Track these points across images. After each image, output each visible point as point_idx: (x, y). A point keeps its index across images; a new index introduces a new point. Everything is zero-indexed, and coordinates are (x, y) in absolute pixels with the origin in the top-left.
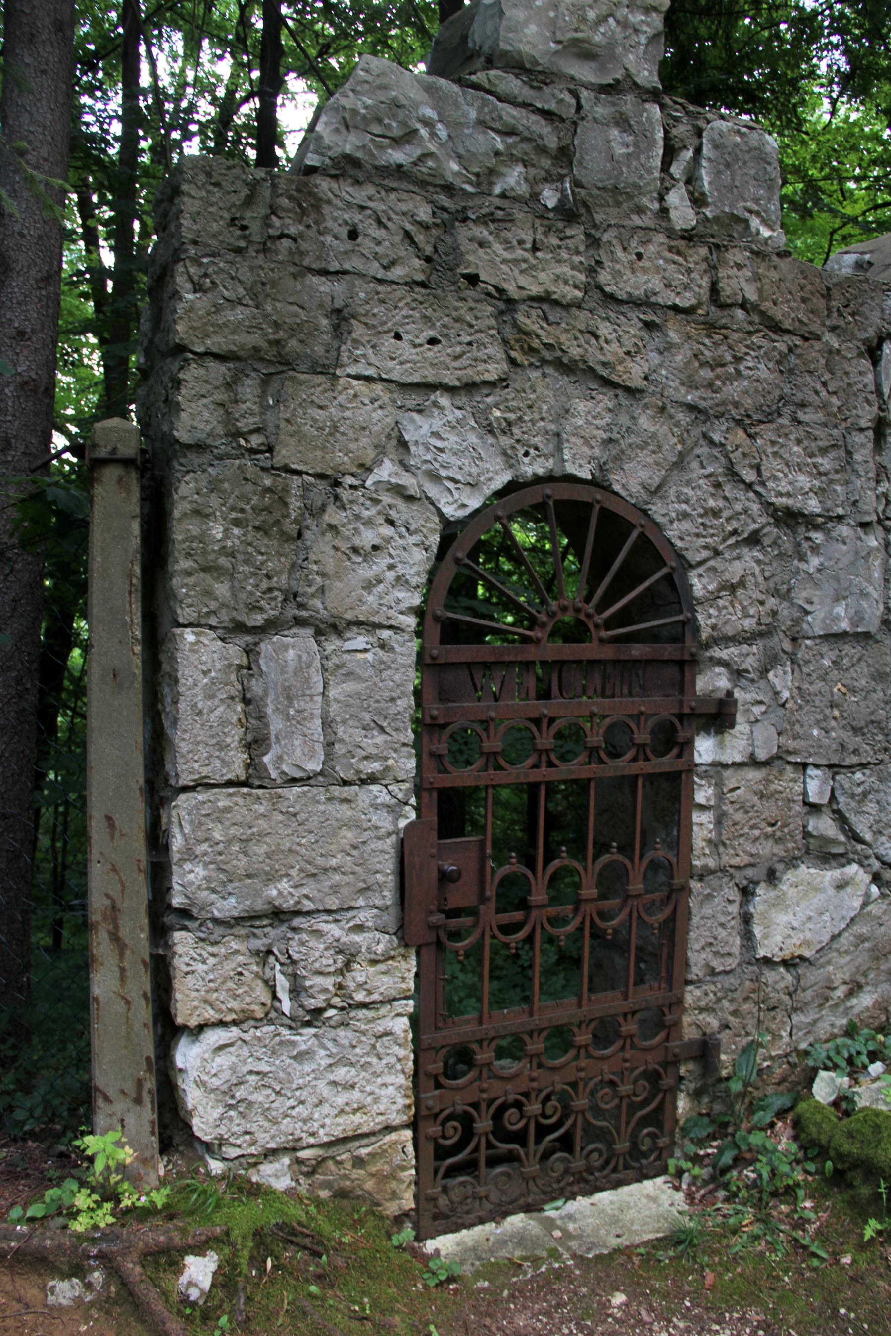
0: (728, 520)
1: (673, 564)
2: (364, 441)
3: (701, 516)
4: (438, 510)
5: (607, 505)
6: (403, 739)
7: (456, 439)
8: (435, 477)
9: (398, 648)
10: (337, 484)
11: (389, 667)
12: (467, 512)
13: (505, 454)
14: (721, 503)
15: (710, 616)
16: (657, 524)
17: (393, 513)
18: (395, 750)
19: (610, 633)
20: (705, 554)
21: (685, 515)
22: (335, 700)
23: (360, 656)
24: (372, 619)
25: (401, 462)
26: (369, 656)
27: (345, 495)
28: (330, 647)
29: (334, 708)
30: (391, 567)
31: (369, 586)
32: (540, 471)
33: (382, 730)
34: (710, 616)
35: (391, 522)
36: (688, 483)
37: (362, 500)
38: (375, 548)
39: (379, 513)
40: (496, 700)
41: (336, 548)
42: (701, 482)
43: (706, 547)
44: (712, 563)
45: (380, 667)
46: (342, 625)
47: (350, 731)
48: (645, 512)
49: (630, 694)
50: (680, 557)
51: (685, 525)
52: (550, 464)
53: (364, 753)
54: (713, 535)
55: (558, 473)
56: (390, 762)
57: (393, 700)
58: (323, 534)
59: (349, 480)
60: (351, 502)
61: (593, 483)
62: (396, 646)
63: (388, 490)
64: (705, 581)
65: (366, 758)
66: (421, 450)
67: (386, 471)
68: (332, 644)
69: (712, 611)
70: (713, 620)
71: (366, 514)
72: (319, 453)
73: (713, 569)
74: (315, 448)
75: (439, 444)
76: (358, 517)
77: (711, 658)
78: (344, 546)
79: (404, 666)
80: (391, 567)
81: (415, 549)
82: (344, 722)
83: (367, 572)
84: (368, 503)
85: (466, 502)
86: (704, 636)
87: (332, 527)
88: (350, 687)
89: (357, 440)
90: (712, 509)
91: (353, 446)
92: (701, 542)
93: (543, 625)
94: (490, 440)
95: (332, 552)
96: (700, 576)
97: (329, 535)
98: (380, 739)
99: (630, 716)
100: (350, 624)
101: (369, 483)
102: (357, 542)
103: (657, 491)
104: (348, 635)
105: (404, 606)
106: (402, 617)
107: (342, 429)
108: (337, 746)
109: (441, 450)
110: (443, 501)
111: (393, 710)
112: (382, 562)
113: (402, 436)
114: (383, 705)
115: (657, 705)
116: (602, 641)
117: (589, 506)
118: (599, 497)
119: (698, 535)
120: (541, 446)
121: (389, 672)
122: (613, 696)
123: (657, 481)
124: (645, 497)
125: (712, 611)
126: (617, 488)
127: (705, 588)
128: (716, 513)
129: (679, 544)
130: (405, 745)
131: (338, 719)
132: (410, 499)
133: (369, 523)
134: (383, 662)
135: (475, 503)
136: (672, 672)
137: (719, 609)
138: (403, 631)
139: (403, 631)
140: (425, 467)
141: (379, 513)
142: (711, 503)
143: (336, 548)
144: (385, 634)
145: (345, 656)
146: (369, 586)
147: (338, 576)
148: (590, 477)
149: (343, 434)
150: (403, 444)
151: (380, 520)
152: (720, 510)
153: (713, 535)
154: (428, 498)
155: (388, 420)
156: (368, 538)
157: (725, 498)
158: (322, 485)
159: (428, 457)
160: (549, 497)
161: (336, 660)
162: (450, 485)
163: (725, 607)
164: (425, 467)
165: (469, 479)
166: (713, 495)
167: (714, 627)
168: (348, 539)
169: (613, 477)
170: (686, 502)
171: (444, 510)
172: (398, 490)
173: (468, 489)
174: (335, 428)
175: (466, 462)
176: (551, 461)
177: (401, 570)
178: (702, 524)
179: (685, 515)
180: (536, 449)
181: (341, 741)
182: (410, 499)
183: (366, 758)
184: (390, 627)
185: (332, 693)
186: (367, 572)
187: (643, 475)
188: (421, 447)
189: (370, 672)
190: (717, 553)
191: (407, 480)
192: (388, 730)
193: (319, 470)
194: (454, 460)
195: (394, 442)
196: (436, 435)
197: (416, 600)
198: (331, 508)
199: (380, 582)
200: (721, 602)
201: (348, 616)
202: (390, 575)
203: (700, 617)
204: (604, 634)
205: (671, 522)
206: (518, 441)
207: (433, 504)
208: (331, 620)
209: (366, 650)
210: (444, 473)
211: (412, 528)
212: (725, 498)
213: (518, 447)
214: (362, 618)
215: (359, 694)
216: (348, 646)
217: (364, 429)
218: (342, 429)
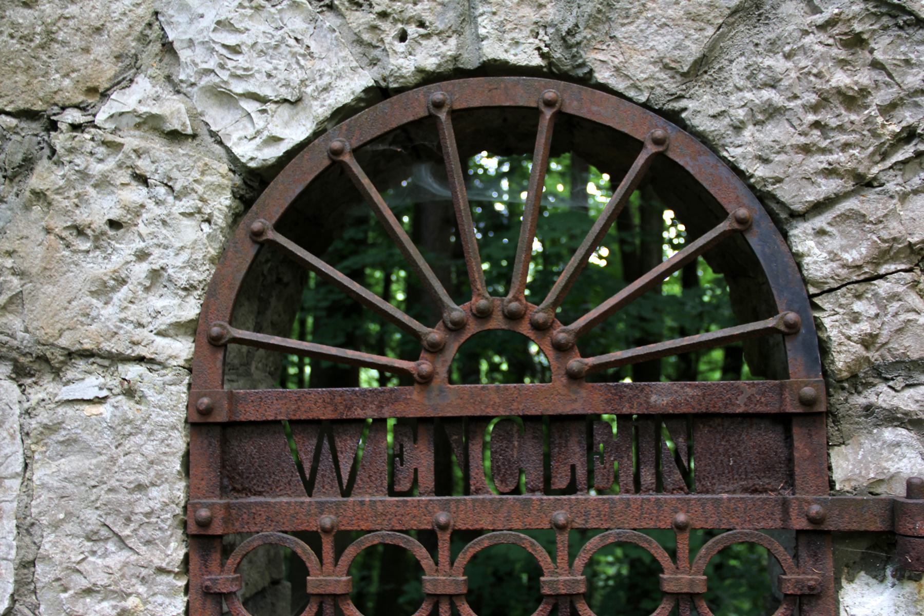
0: (889, 109)
1: (742, 212)
2: (99, 50)
3: (815, 108)
4: (228, 151)
5: (572, 108)
6: (158, 561)
7: (264, 27)
8: (224, 97)
9: (152, 396)
10: (53, 126)
11: (139, 430)
12: (278, 151)
13: (360, 42)
14: (865, 77)
15: (856, 318)
16: (702, 137)
17: (144, 165)
18: (143, 580)
19: (592, 361)
20: (828, 187)
21: (772, 112)
22: (43, 485)
23: (89, 410)
24: (106, 346)
25: (168, 78)
26: (105, 410)
27: (60, 140)
28: (36, 395)
29: (41, 500)
30: (142, 256)
31: (103, 290)
32: (430, 63)
33: (122, 541)
34: (856, 318)
35: (142, 180)
36: (773, 47)
37: (90, 146)
38: (114, 224)
39: (120, 166)
40: (346, 493)
41: (48, 231)
42: (807, 40)
43: (830, 172)
44: (851, 204)
45: (125, 430)
46: (58, 357)
47: (67, 541)
48: (674, 117)
49: (660, 487)
50: (764, 198)
51: (777, 131)
52: (450, 47)
53: (85, 583)
54: (846, 146)
55: (470, 61)
56: (131, 602)
57: (140, 487)
58: (27, 208)
59: (74, 116)
60: (71, 151)
61: (550, 71)
62: (149, 393)
63: (138, 126)
64: (834, 243)
65: (88, 591)
66: (199, 54)
67: (138, 96)
68: (46, 389)
69: (858, 306)
70: (865, 327)
71: (97, 169)
72: (21, 78)
73: (859, 217)
74: (15, 70)
75: (232, 39)
76: (84, 175)
77: (869, 409)
78: (59, 224)
79: (161, 427)
80: (142, 256)
81: (186, 222)
82: (56, 526)
83: (98, 267)
84: (101, 151)
85: (278, 132)
86: (841, 361)
87: (39, 195)
88: (72, 463)
89: (86, 50)
90: (839, 92)
91: (79, 61)
92: (818, 162)
93: (436, 349)
94: (330, 20)
95: (41, 236)
96: (821, 233)
97: (37, 209)
98: (117, 558)
99: (657, 533)
100: (70, 355)
101: (100, 118)
102: (82, 217)
103: (700, 69)
104: (70, 375)
105: (162, 322)
106: (160, 340)
107: (61, 36)
108: (39, 568)
109: (235, 50)
110: (235, 137)
111: (143, 507)
112: (124, 248)
113: (165, 36)
114: (123, 496)
115: (728, 507)
116: (574, 377)
117: (534, 113)
118: (550, 95)
119: (806, 149)
120: (428, 18)
121: (138, 439)
122: (572, 489)
123: (694, 50)
124: (672, 87)
125: (858, 306)
126: (603, 76)
127: (834, 257)
128: (852, 99)
129: (760, 171)
130: (161, 570)
131: (45, 520)
132: (175, 136)
133: (103, 183)
134: (127, 421)
135: (296, 131)
136: (768, 439)
137: (882, 303)
138: (163, 365)
139: (163, 365)
140: (205, 81)
141: (120, 166)
142: (840, 79)
143: (48, 231)
144: (133, 371)
145: (61, 410)
146: (103, 290)
147: (47, 273)
148: (537, 61)
149: (64, 43)
150: (168, 48)
151: (124, 177)
152: (864, 92)
153: (846, 146)
154: (213, 134)
155: (140, 11)
156: (101, 208)
157: (876, 65)
158: (30, 128)
159: (212, 64)
160: (438, 105)
161: (43, 417)
162: (251, 106)
163: (895, 297)
164: (205, 81)
165: (285, 93)
166: (842, 63)
167: (868, 341)
168: (66, 212)
169: (591, 57)
170: (773, 84)
171: (237, 151)
172: (151, 123)
173: (285, 110)
174: (50, 37)
175: (282, 65)
176: (453, 42)
177: (157, 260)
178: (816, 125)
179: (772, 112)
180: (422, 24)
181: (47, 559)
182: (175, 136)
183: (88, 591)
184: (141, 359)
185: (39, 474)
186: (98, 267)
187: (662, 43)
188: (199, 50)
189: (107, 438)
190: (863, 183)
191: (175, 111)
192: (131, 542)
193: (21, 105)
194: (262, 65)
195: (156, 47)
196: (222, 25)
197: (191, 309)
198: (43, 165)
199: (123, 282)
200: (882, 287)
201: (64, 342)
202: (141, 270)
203: (827, 322)
204: (576, 362)
205: (738, 128)
206: (383, 15)
207: (221, 143)
208: (39, 350)
209: (100, 401)
210: (238, 87)
211: (177, 187)
212: (876, 65)
213: (385, 25)
214: (88, 345)
215: (83, 476)
216: (67, 393)
217: (98, 30)
218: (61, 36)
